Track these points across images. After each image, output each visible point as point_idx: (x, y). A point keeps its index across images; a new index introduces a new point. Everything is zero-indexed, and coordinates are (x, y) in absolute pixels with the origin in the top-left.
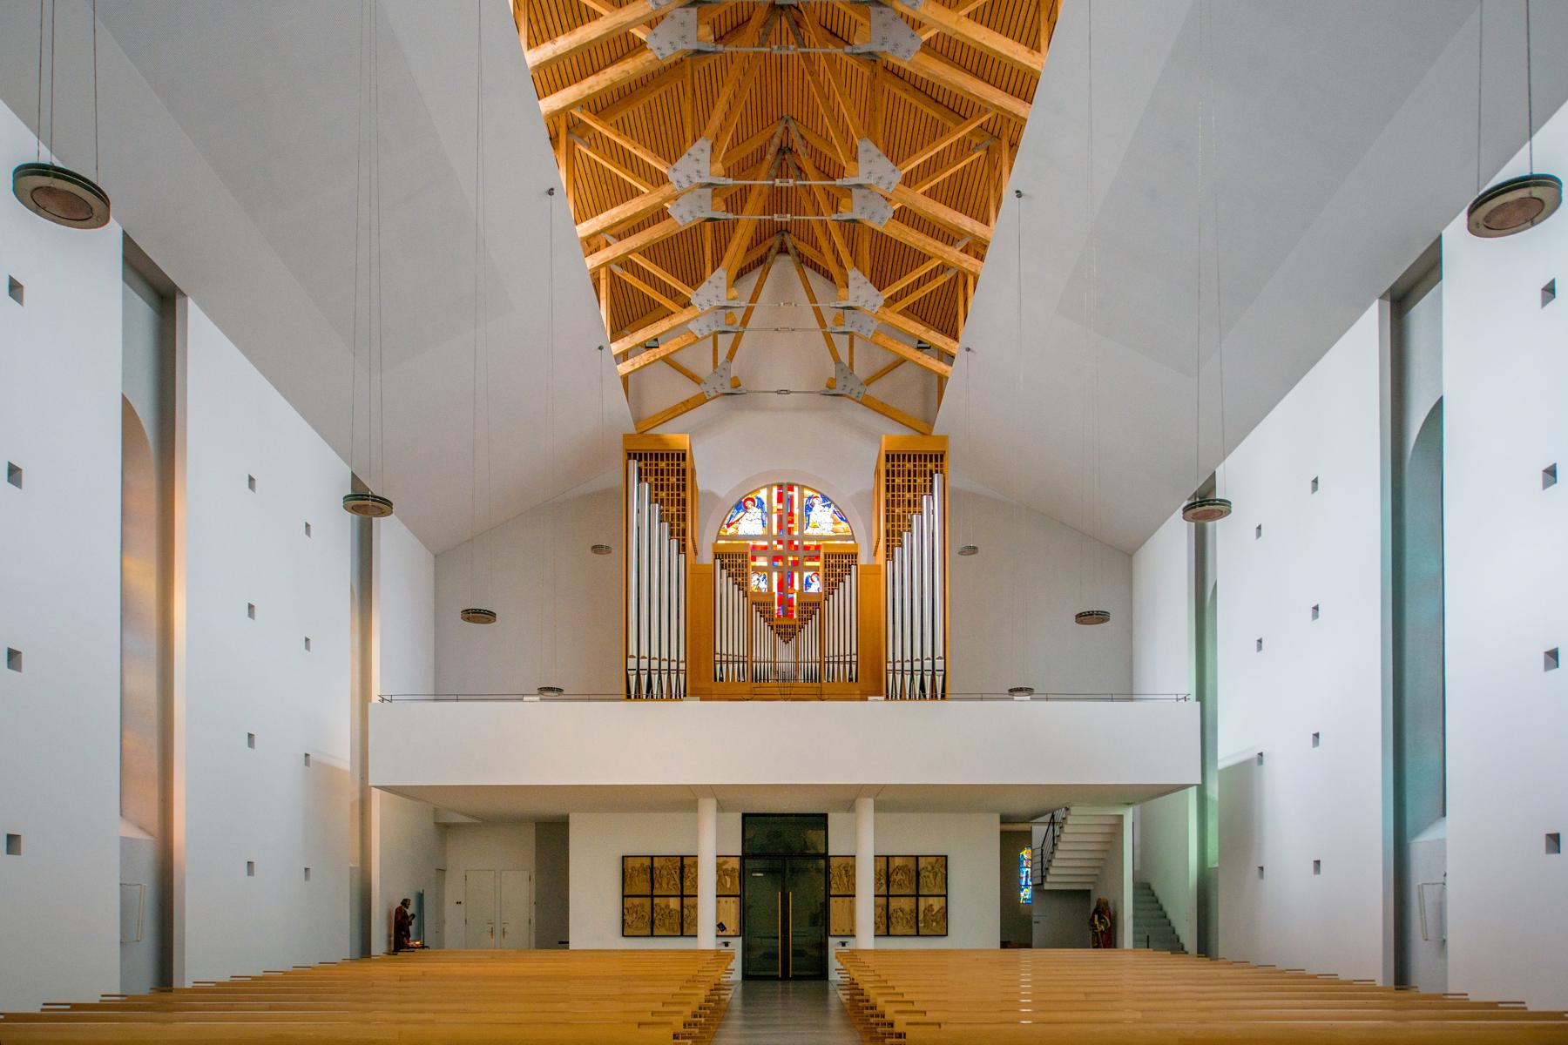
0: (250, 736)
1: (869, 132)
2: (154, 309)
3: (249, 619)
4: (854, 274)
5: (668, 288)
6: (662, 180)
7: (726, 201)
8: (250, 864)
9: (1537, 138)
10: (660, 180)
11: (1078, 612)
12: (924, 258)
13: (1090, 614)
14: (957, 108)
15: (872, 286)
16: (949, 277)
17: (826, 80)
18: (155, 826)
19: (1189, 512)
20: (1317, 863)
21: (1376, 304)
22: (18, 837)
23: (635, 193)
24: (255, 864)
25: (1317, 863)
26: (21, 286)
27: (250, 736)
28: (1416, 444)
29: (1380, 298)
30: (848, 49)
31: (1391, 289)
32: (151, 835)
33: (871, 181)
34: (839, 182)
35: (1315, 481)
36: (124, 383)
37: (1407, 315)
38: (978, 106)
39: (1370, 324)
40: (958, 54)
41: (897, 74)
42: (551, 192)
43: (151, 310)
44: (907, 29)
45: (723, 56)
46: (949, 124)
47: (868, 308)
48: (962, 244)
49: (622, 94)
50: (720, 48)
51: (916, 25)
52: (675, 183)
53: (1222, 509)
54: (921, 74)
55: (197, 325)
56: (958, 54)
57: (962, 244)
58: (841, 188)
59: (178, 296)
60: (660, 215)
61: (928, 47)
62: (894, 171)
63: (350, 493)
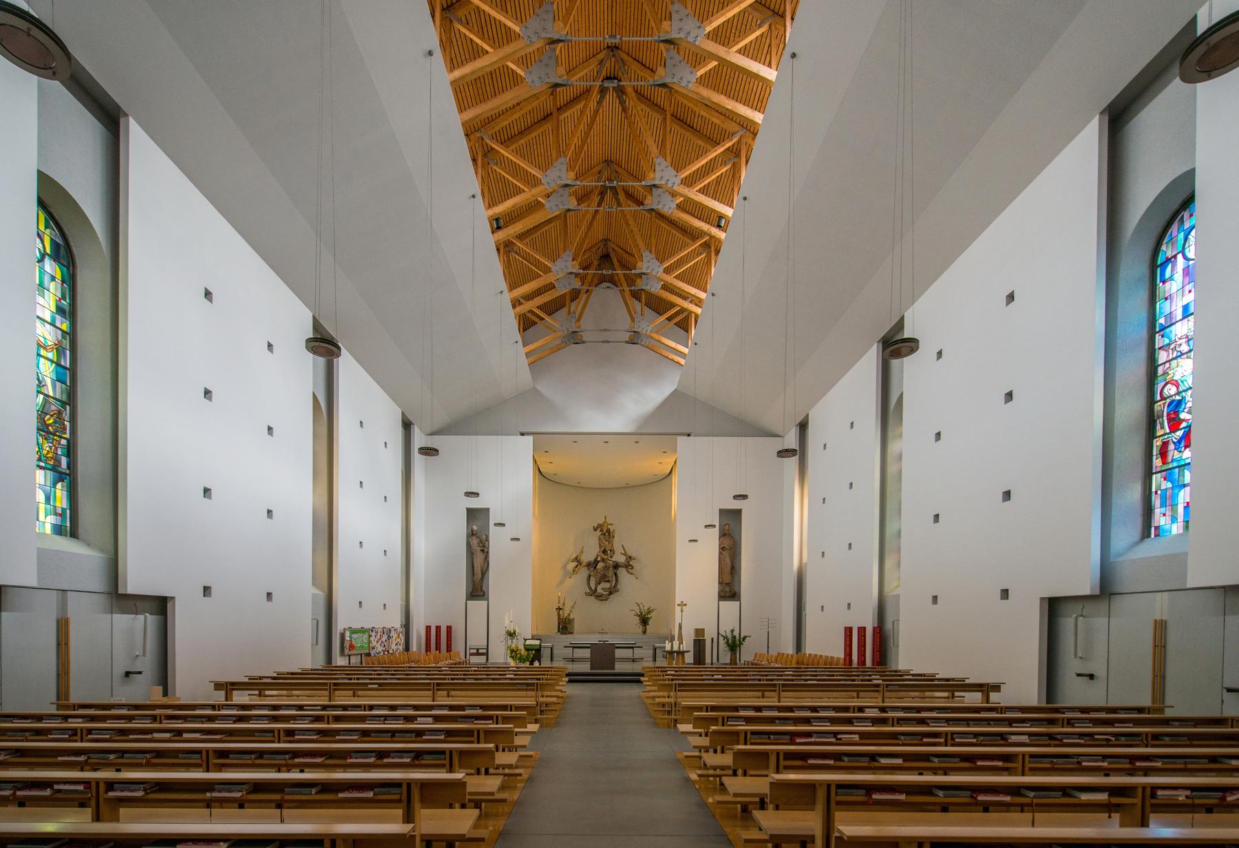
0: (361, 543)
1: (662, 153)
2: (106, 127)
3: (269, 436)
4: (646, 254)
5: (529, 175)
6: (547, 270)
7: (581, 279)
8: (360, 602)
9: (915, 304)
10: (534, 182)
11: (734, 495)
12: (673, 305)
13: (787, 450)
14: (693, 234)
15: (672, 169)
16: (685, 315)
17: (639, 127)
18: (326, 589)
19: (886, 351)
20: (849, 604)
21: (876, 345)
22: (271, 593)
23: (520, 191)
24: (212, 589)
25: (849, 604)
26: (211, 293)
27: (361, 543)
28: (1133, 235)
29: (1101, 113)
30: (641, 207)
31: (1109, 106)
32: (324, 592)
33: (649, 271)
34: (633, 272)
35: (852, 423)
36: (40, 155)
37: (1125, 128)
38: (702, 233)
39: (871, 358)
40: (693, 211)
41: (661, 216)
42: (474, 196)
43: (109, 134)
44: (670, 198)
45: (580, 188)
46: (708, 147)
47: (654, 273)
48: (690, 300)
49: (530, 206)
50: (578, 183)
51: (674, 195)
52: (546, 184)
53: (911, 345)
54: (673, 218)
55: (136, 137)
56: (693, 211)
57: (690, 300)
58: (635, 274)
59: (121, 115)
60: (534, 206)
61: (679, 206)
62: (659, 266)
63: (312, 337)
